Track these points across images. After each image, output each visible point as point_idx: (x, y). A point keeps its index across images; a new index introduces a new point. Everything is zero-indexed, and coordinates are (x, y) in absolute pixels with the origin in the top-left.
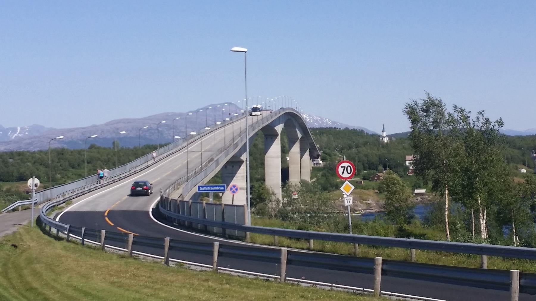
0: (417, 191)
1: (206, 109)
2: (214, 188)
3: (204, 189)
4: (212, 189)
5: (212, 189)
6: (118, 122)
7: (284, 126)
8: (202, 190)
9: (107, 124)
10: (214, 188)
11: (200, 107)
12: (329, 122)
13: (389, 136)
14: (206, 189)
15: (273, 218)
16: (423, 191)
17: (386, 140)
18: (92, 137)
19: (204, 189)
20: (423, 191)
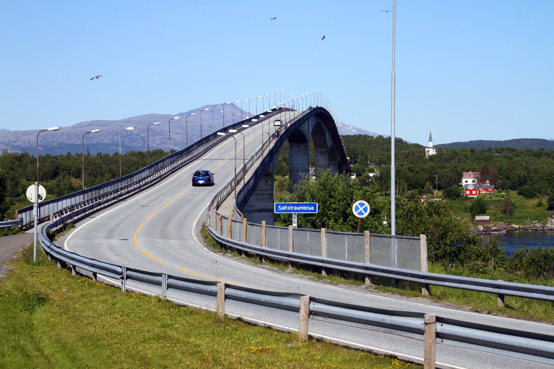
0: (478, 218)
1: (202, 110)
2: (300, 208)
3: (283, 208)
4: (296, 208)
5: (296, 208)
6: (152, 116)
7: (300, 131)
8: (281, 211)
9: (74, 127)
10: (300, 208)
11: (193, 109)
12: (353, 130)
13: (437, 148)
14: (287, 208)
15: (291, 228)
16: (487, 218)
17: (432, 152)
18: (92, 131)
19: (283, 208)
20: (487, 218)
